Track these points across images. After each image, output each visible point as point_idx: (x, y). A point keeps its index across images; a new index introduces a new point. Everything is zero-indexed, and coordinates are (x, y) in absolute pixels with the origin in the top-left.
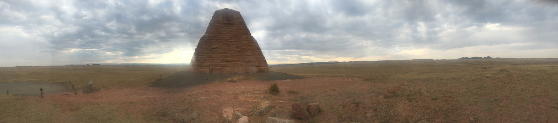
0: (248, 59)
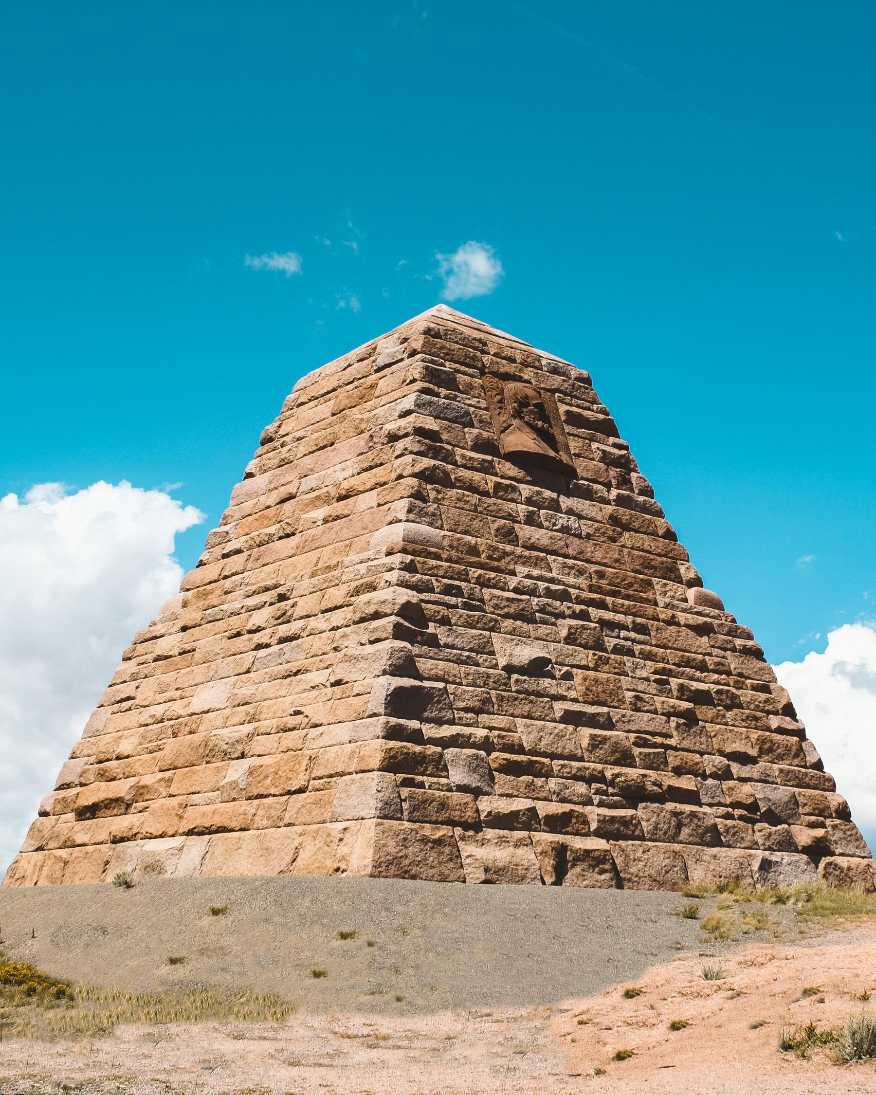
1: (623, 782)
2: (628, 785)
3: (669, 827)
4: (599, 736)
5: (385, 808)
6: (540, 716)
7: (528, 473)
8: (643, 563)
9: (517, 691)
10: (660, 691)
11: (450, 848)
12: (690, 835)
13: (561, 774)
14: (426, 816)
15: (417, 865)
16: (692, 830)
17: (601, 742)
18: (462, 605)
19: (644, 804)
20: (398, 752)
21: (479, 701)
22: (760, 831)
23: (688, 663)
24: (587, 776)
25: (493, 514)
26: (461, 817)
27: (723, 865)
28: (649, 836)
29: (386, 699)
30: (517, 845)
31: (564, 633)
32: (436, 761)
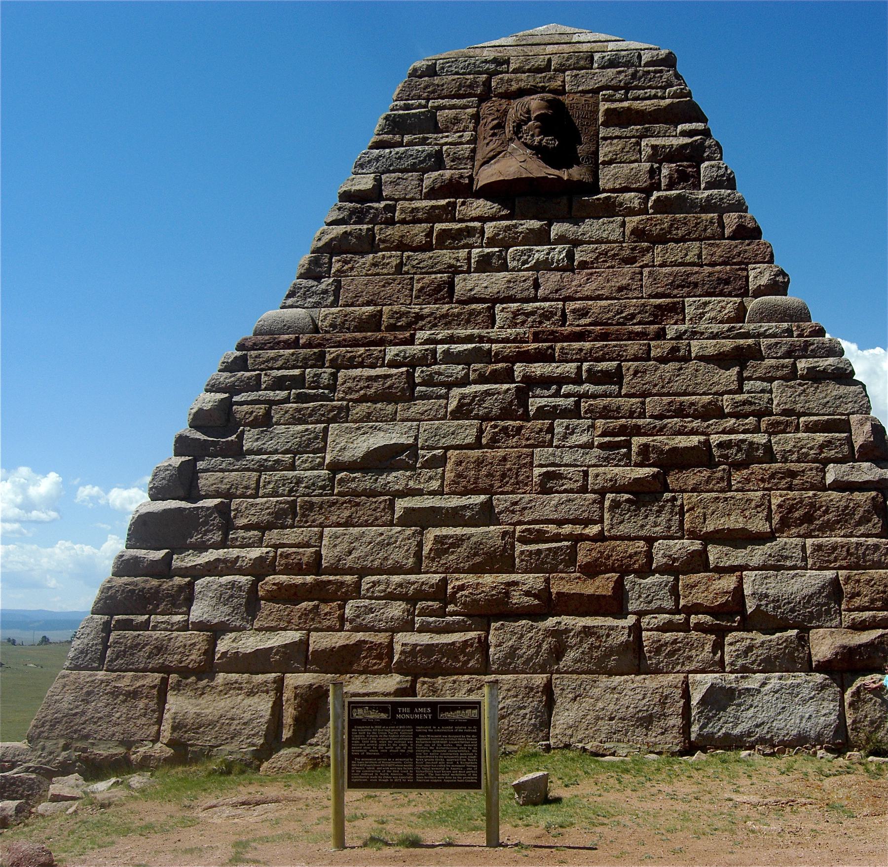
0: (728, 582)
1: (466, 596)
2: (474, 600)
3: (537, 653)
4: (452, 537)
5: (78, 658)
6: (366, 521)
7: (504, 205)
8: (673, 281)
9: (340, 494)
10: (606, 459)
11: (147, 701)
12: (576, 661)
13: (369, 594)
14: (133, 664)
15: (96, 723)
16: (583, 653)
17: (452, 545)
18: (294, 398)
19: (499, 624)
20: (118, 591)
21: (269, 514)
22: (731, 644)
23: (680, 412)
24: (410, 592)
25: (424, 270)
26: (181, 663)
27: (625, 701)
28: (496, 666)
29: (129, 530)
30: (252, 692)
31: (453, 405)
32: (172, 596)
